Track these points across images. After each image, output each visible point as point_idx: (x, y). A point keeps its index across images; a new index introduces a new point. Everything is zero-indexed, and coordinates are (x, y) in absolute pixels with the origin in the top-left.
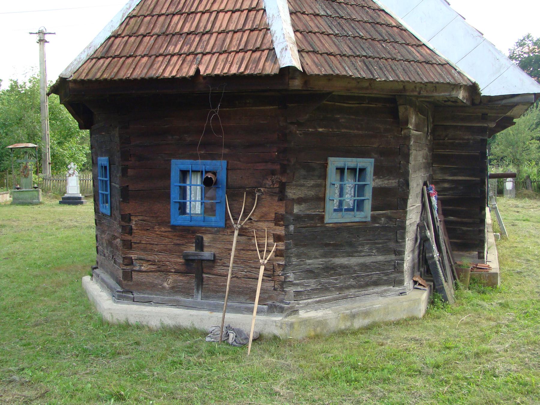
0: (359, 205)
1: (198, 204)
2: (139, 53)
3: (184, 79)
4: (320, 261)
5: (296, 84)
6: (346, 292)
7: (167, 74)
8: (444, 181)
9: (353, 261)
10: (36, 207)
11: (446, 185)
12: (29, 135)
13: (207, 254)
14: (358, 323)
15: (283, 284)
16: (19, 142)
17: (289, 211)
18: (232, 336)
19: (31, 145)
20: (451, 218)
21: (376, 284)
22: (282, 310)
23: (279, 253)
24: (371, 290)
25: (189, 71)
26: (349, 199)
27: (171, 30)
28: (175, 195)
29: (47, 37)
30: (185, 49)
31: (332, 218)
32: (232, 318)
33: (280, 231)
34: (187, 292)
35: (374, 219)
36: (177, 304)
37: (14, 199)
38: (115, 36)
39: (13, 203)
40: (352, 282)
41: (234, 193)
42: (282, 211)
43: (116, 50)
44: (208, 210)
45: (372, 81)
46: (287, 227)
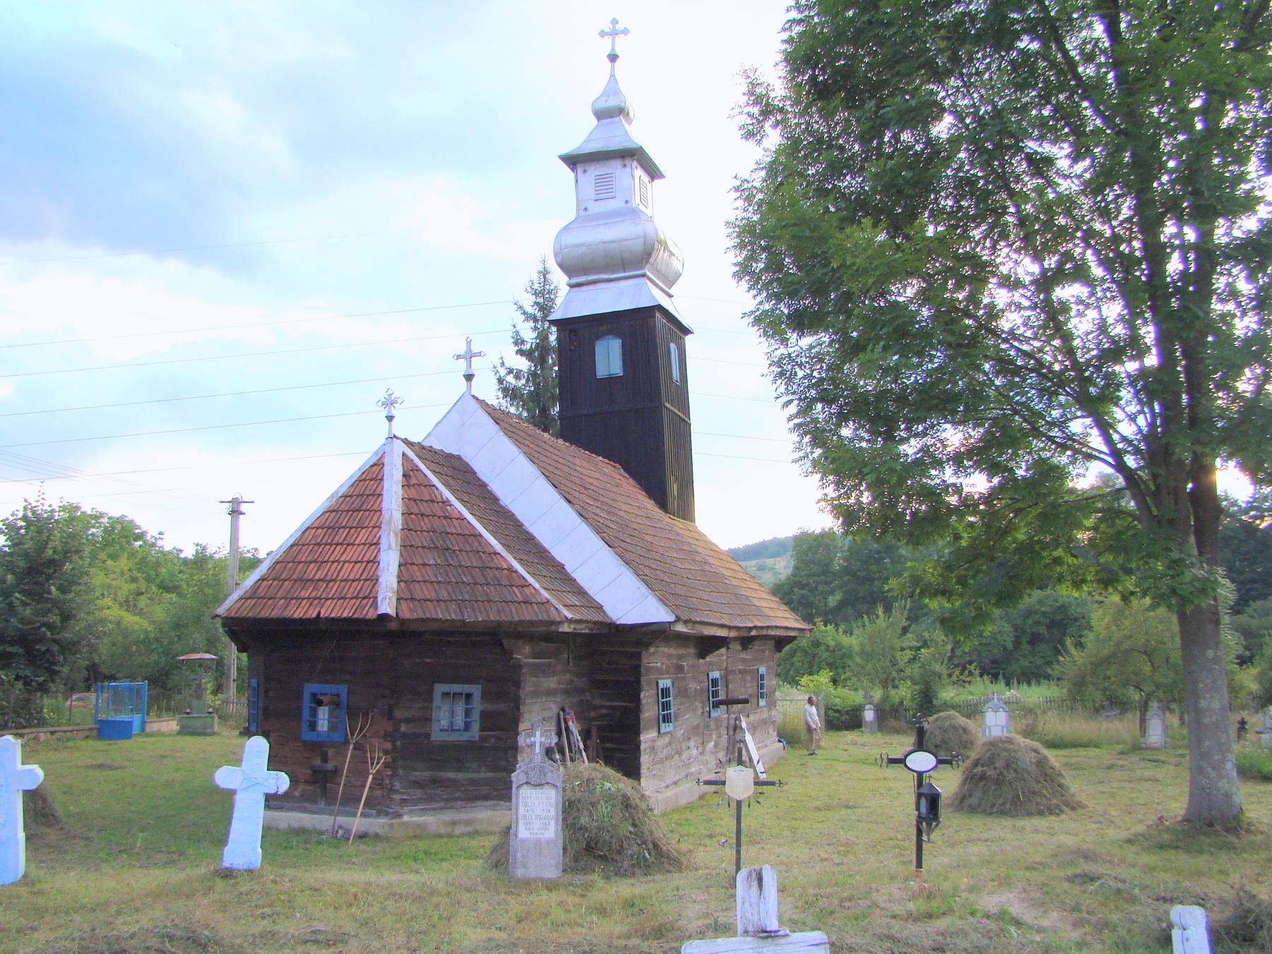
0: (467, 727)
1: (326, 723)
2: (279, 595)
3: (308, 620)
4: (427, 774)
5: (393, 626)
6: (454, 804)
7: (295, 616)
8: (603, 707)
9: (460, 776)
10: (208, 738)
11: (604, 711)
12: (208, 640)
13: (330, 766)
14: (458, 830)
15: (392, 790)
16: (195, 650)
17: (397, 729)
18: (340, 832)
19: (207, 656)
20: (609, 745)
21: (486, 798)
22: (387, 814)
23: (386, 765)
24: (479, 803)
25: (312, 614)
26: (459, 720)
27: (305, 577)
28: (306, 714)
29: (243, 508)
30: (313, 595)
31: (437, 736)
32: (342, 820)
33: (388, 746)
34: (314, 800)
35: (483, 739)
36: (304, 810)
37: (182, 727)
38: (345, 496)
39: (179, 733)
40: (458, 794)
41: (352, 713)
42: (390, 729)
43: (261, 592)
44: (333, 727)
45: (463, 622)
46: (394, 743)
